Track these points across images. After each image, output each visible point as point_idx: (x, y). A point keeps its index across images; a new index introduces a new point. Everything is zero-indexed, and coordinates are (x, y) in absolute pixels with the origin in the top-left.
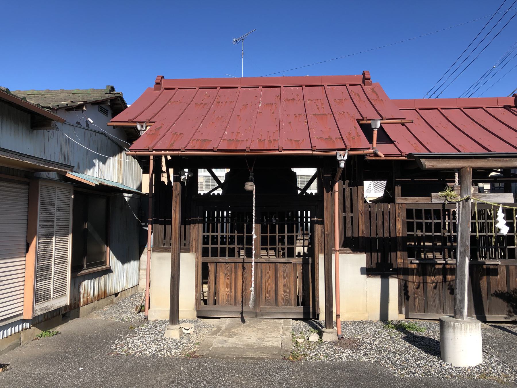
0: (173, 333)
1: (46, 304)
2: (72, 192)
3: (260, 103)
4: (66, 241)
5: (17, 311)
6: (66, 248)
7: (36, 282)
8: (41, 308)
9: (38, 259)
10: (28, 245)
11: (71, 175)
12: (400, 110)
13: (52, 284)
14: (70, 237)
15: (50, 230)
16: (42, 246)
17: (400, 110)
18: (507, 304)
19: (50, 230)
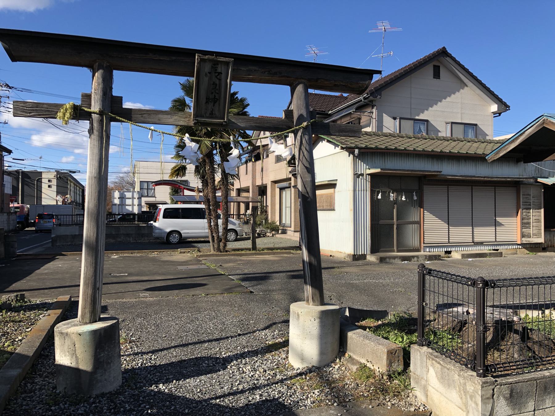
0: (302, 311)
1: (528, 239)
2: (542, 188)
3: (151, 408)
4: (540, 212)
5: (515, 239)
6: (540, 216)
7: (522, 229)
8: (525, 240)
9: (522, 219)
10: (518, 213)
11: (539, 180)
12: (247, 174)
13: (531, 231)
14: (542, 210)
15: (529, 207)
16: (524, 214)
17: (247, 174)
18: (479, 381)
19: (529, 207)
